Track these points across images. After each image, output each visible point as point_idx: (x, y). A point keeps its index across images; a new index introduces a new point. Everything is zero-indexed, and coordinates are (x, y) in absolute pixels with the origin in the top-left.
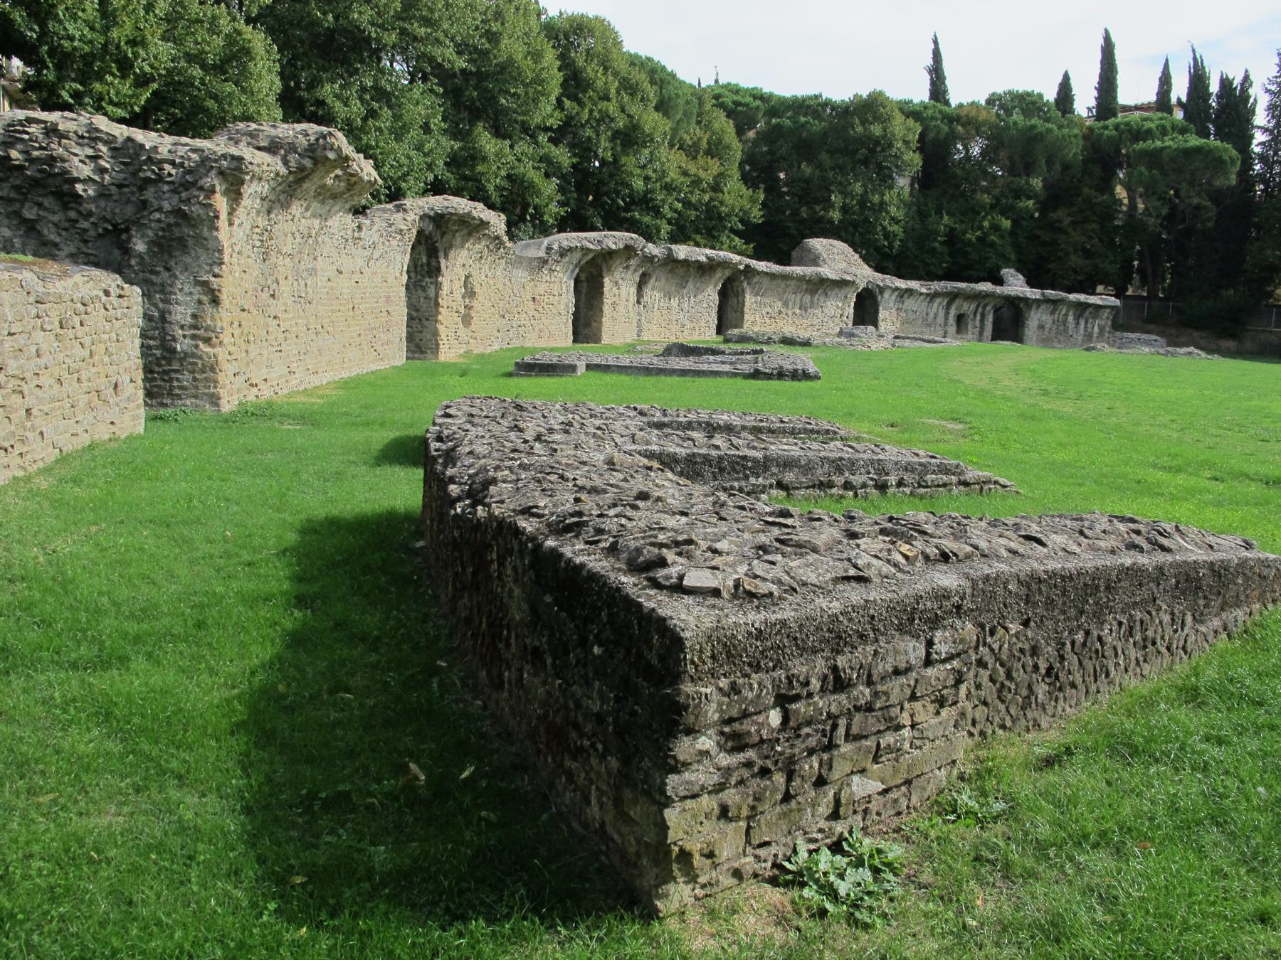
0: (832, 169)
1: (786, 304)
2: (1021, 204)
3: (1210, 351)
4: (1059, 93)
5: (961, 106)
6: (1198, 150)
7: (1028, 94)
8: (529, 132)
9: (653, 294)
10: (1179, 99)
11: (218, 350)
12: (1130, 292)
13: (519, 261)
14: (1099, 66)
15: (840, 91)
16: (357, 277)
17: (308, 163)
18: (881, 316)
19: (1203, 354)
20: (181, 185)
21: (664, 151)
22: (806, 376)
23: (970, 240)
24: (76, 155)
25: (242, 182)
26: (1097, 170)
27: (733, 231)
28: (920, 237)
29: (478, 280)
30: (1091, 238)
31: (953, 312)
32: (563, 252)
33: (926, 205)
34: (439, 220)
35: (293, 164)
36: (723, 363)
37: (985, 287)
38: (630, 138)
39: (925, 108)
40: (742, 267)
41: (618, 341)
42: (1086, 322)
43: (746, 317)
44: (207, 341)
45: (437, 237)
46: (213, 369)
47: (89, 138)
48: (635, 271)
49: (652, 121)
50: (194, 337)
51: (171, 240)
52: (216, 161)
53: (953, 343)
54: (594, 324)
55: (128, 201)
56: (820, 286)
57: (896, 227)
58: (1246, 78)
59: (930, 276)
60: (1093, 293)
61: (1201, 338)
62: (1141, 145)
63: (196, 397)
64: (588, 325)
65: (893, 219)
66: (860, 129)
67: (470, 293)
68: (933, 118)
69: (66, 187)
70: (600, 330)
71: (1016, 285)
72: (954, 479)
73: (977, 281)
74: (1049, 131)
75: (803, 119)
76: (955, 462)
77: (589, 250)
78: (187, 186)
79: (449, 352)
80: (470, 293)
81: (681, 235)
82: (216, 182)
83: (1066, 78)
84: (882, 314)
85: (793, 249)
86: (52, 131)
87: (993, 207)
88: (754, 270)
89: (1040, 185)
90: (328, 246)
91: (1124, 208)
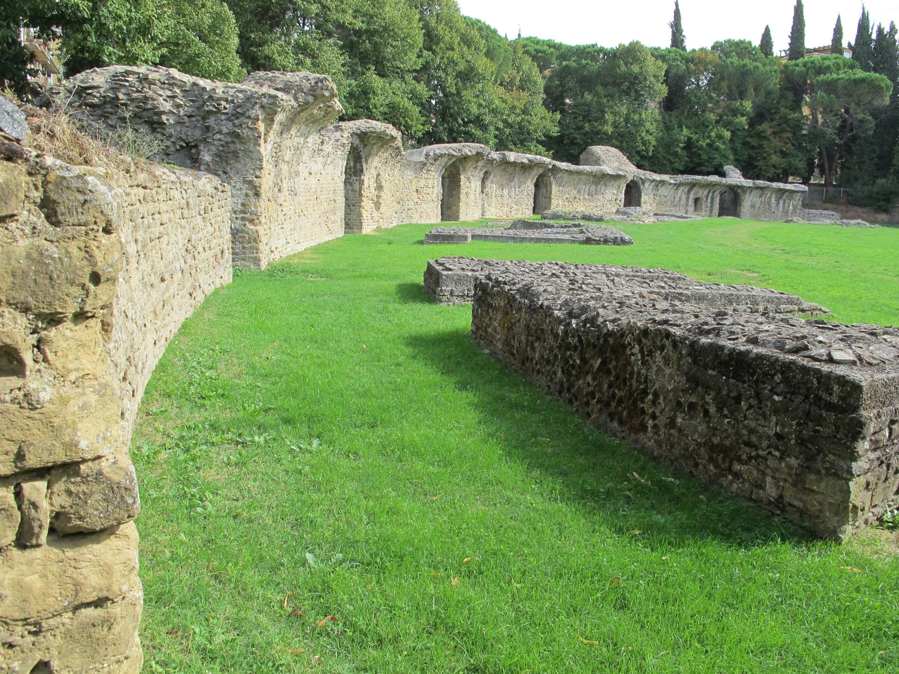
0: (605, 96)
1: (579, 192)
2: (737, 120)
3: (873, 222)
4: (762, 41)
5: (694, 51)
6: (863, 80)
7: (742, 42)
8: (400, 74)
9: (492, 187)
10: (849, 43)
11: (258, 228)
12: (812, 182)
13: (409, 164)
14: (792, 20)
15: (610, 41)
16: (318, 176)
17: (311, 99)
18: (643, 200)
19: (868, 224)
20: (233, 115)
21: (490, 87)
22: (623, 242)
23: (702, 146)
24: (161, 96)
25: (276, 113)
26: (790, 95)
27: (538, 142)
28: (667, 144)
29: (384, 176)
30: (786, 143)
31: (692, 196)
32: (437, 157)
33: (670, 121)
34: (363, 137)
35: (301, 100)
36: (564, 233)
37: (714, 178)
38: (467, 76)
39: (669, 52)
40: (550, 167)
41: (470, 219)
42: (784, 202)
43: (553, 201)
44: (252, 221)
45: (361, 148)
46: (255, 240)
47: (168, 84)
48: (481, 170)
49: (482, 64)
50: (243, 219)
51: (228, 153)
52: (258, 98)
53: (697, 219)
54: (454, 208)
55: (195, 127)
56: (603, 178)
57: (650, 137)
58: (892, 28)
59: (676, 172)
60: (786, 182)
61: (863, 212)
62: (822, 77)
63: (244, 260)
64: (449, 208)
65: (647, 131)
66: (624, 68)
67: (380, 187)
68: (674, 60)
69: (155, 118)
70: (458, 211)
71: (735, 177)
72: (796, 308)
73: (708, 174)
74: (756, 68)
75: (584, 62)
76: (796, 297)
77: (453, 155)
78: (237, 115)
79: (368, 228)
80: (380, 187)
81: (501, 145)
82: (259, 112)
83: (767, 30)
84: (644, 198)
85: (581, 153)
86: (143, 79)
87: (717, 122)
88: (559, 168)
89: (751, 105)
90: (307, 153)
91: (809, 122)
